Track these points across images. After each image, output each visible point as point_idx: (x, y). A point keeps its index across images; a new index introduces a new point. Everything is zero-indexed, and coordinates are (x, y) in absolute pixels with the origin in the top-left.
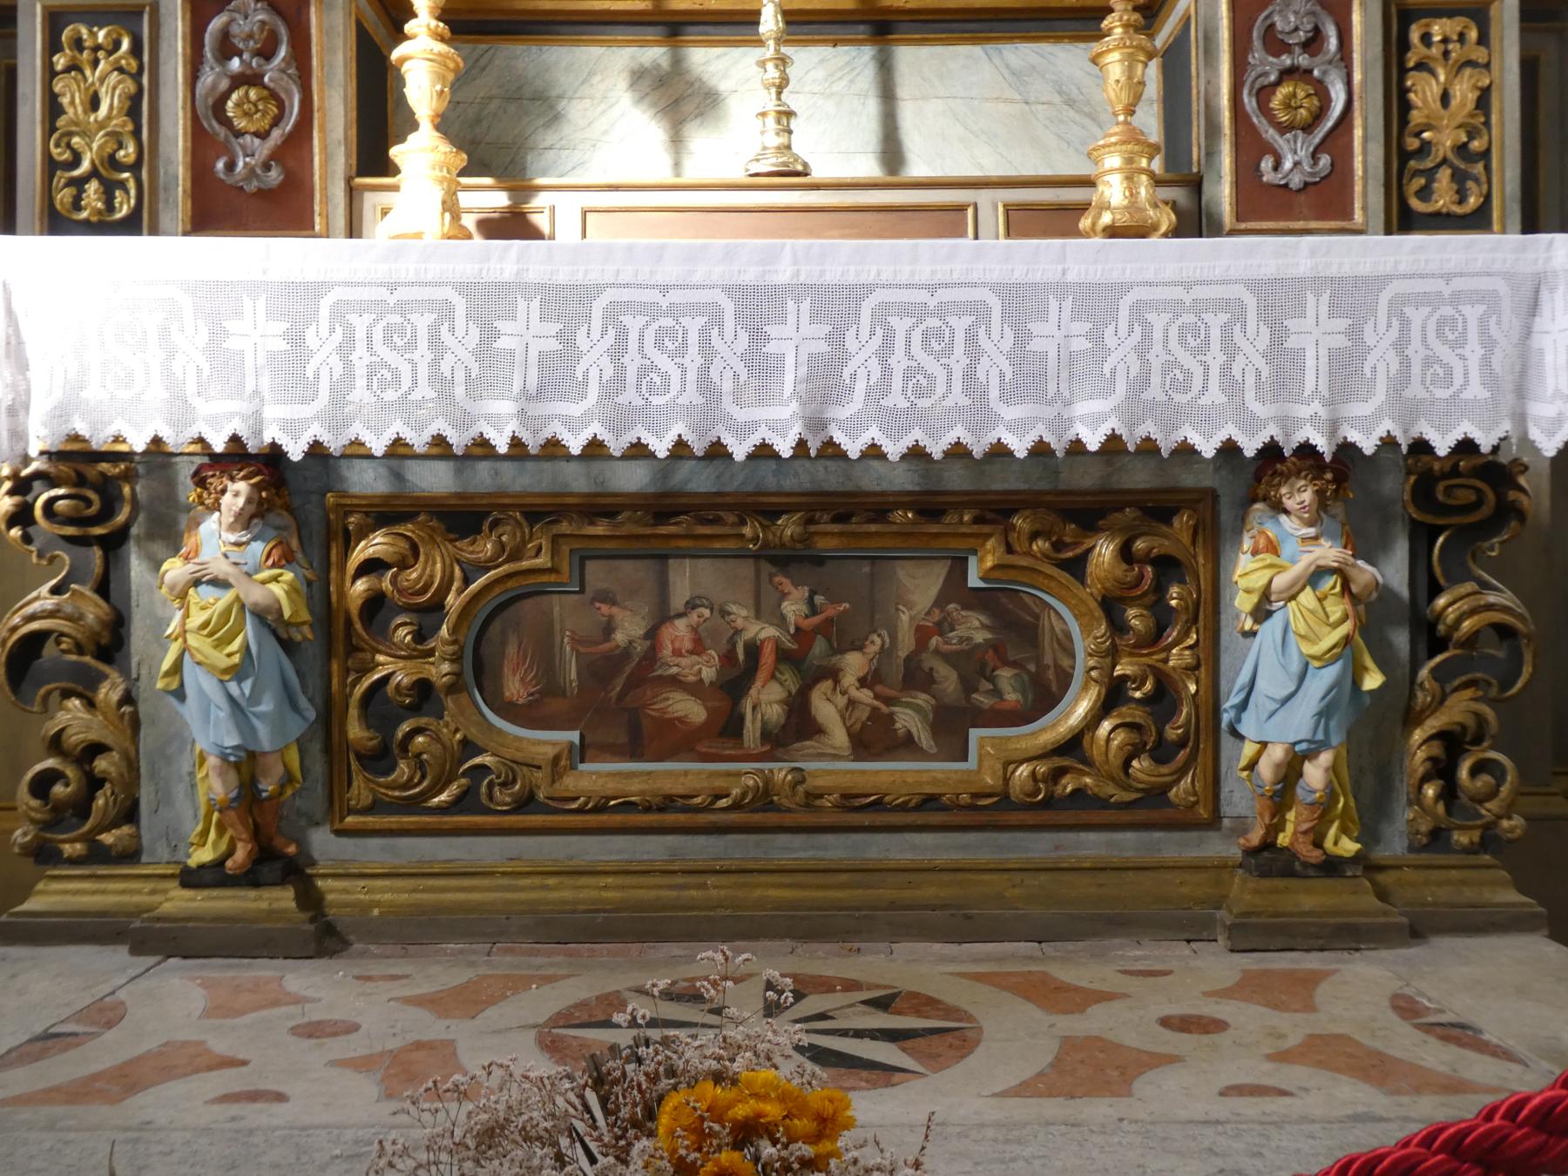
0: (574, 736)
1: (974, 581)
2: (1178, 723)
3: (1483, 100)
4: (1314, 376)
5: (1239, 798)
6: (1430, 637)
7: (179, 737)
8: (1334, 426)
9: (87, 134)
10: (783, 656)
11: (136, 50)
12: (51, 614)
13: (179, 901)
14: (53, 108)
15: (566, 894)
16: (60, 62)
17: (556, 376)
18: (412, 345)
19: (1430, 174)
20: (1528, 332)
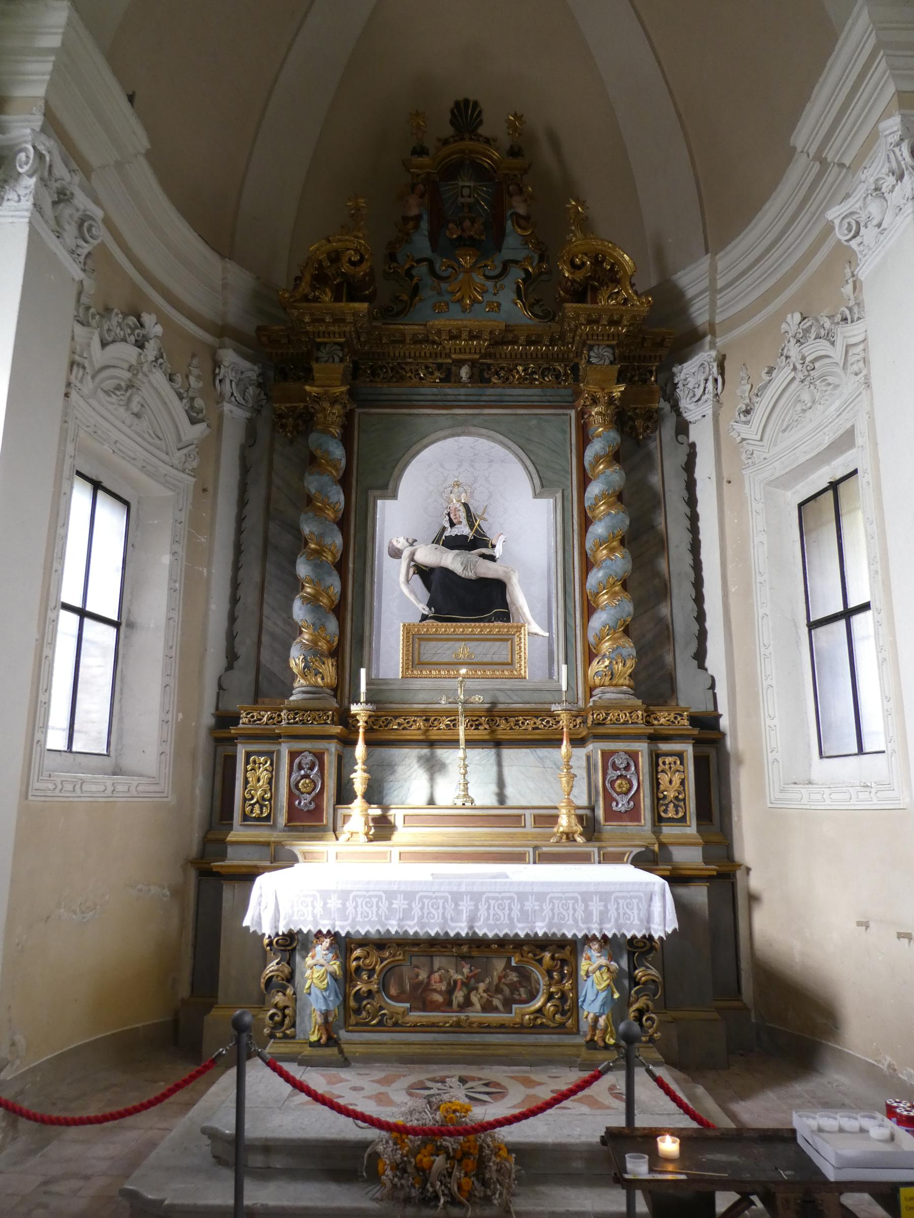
0: (408, 1005)
1: (513, 964)
2: (568, 1005)
3: (682, 783)
4: (595, 917)
5: (585, 1026)
6: (634, 982)
7: (307, 1004)
8: (601, 930)
9: (256, 790)
10: (463, 983)
11: (271, 764)
12: (276, 971)
13: (308, 1051)
14: (246, 782)
15: (405, 1050)
16: (249, 767)
17: (407, 914)
18: (372, 907)
19: (667, 805)
20: (650, 906)
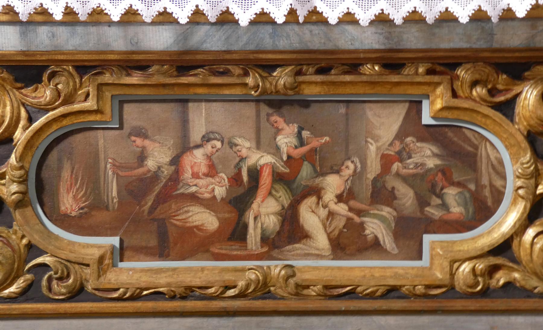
0: (115, 241)
1: (427, 119)
10: (279, 178)
